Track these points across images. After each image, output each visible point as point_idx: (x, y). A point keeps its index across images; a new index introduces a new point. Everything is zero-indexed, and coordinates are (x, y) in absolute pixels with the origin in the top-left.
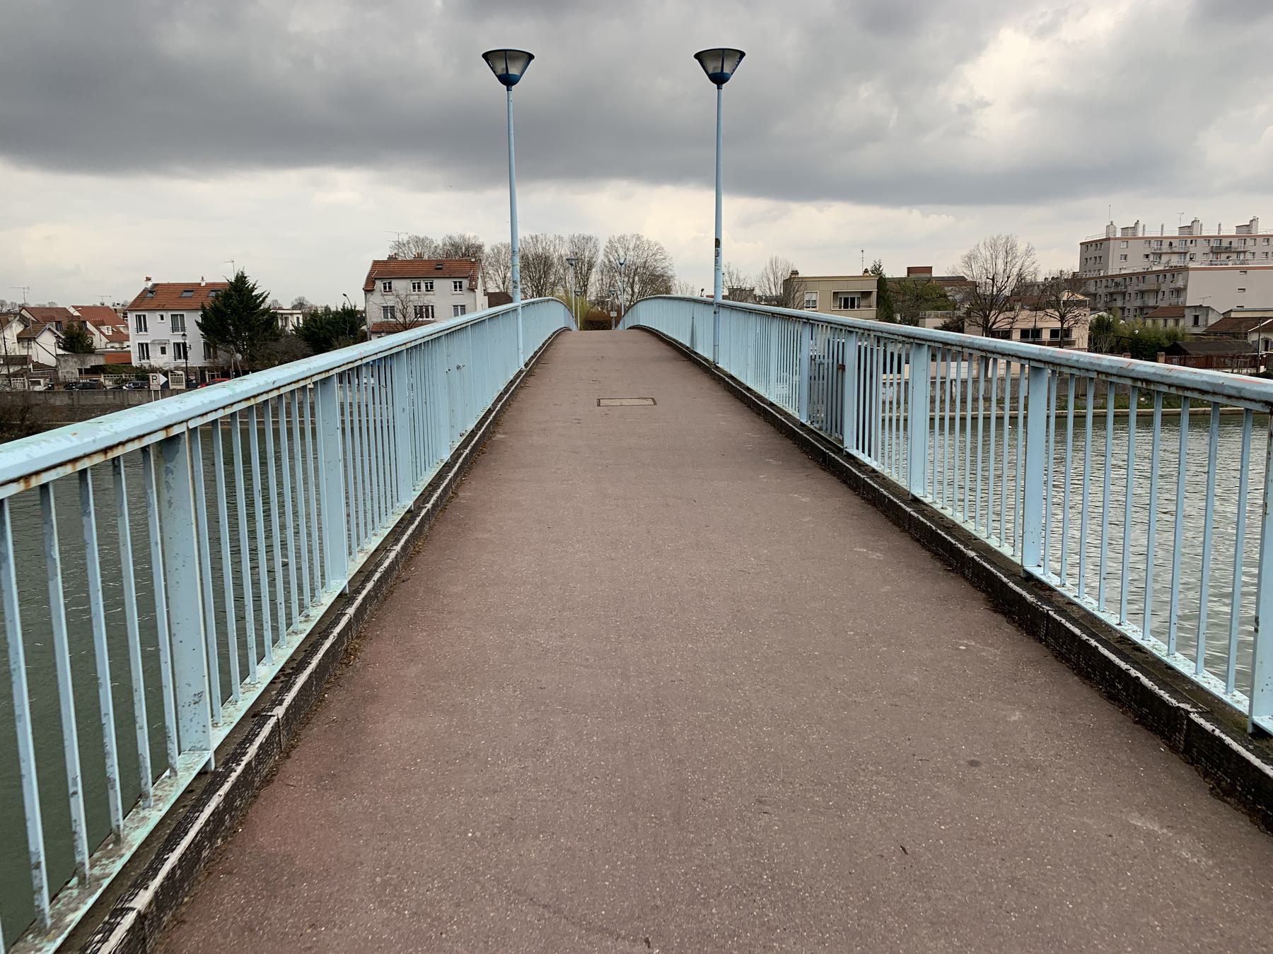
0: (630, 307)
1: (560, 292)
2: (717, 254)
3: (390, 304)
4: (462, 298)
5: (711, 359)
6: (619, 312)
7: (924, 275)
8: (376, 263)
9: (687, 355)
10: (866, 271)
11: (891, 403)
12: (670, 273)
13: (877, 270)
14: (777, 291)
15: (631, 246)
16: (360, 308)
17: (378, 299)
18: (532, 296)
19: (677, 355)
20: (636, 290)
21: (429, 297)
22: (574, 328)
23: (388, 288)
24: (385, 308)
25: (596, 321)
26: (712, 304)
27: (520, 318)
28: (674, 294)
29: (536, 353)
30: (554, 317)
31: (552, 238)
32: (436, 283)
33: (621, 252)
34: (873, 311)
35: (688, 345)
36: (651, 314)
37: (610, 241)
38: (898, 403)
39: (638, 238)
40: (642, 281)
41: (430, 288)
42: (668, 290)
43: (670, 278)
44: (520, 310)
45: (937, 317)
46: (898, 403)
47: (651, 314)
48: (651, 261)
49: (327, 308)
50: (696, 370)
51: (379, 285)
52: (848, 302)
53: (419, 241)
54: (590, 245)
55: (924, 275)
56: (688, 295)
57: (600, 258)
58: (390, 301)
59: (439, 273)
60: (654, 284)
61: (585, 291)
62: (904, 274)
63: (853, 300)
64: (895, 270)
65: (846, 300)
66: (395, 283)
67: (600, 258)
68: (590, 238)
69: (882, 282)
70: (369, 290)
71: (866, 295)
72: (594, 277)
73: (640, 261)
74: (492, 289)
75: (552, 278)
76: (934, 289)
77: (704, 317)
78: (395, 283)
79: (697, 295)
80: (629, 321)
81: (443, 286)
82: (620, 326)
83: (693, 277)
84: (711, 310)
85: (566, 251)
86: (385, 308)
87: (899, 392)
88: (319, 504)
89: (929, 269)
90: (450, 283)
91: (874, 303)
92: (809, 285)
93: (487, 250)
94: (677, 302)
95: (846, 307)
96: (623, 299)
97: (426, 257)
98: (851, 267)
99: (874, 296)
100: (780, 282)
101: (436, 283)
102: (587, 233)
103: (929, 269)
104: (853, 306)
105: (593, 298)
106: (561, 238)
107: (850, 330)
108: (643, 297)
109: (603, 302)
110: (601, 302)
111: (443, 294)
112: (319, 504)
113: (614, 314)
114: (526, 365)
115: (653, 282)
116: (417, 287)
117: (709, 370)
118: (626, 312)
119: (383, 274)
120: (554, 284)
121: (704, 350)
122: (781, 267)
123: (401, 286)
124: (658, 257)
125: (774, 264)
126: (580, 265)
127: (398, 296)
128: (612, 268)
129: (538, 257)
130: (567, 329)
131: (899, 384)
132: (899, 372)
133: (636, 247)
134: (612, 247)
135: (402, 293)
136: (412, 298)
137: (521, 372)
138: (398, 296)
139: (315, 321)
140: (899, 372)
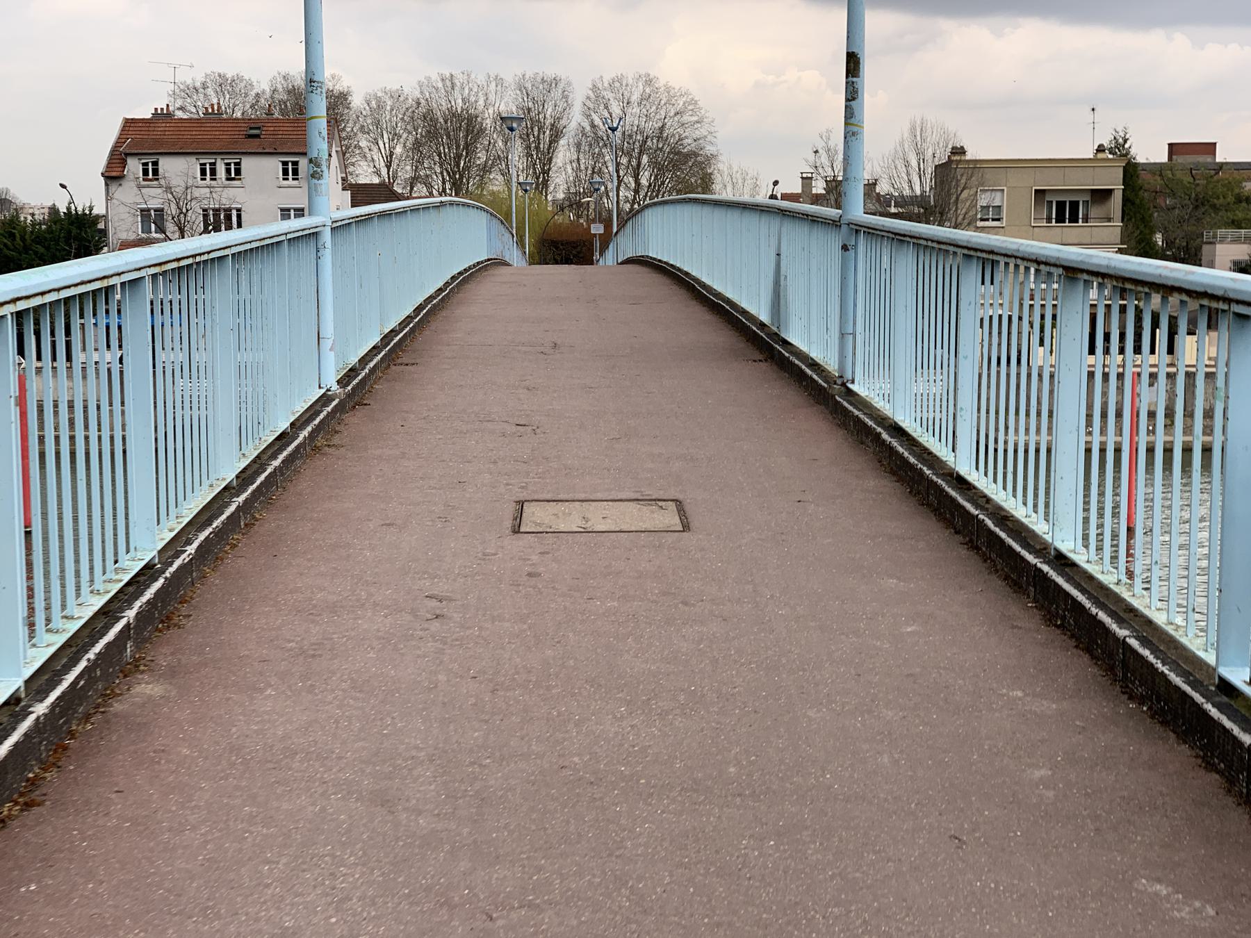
0: (633, 214)
1: (496, 183)
2: (852, 95)
3: (154, 204)
4: (295, 195)
5: (832, 365)
6: (608, 224)
7: (1202, 159)
8: (129, 124)
9: (763, 345)
10: (1101, 149)
11: (1152, 415)
12: (710, 150)
13: (1119, 149)
14: (920, 186)
15: (635, 98)
16: (99, 210)
17: (131, 195)
18: (443, 192)
19: (741, 344)
20: (644, 182)
21: (231, 192)
22: (515, 257)
23: (152, 173)
24: (145, 213)
25: (565, 246)
26: (835, 224)
27: (327, 255)
28: (722, 191)
29: (387, 338)
30: (465, 237)
31: (481, 79)
32: (248, 164)
33: (616, 110)
34: (1115, 228)
35: (764, 317)
36: (668, 235)
37: (594, 88)
38: (1170, 414)
39: (649, 82)
40: (654, 163)
41: (235, 173)
42: (706, 183)
43: (710, 159)
44: (327, 236)
45: (1237, 240)
46: (1170, 414)
47: (668, 235)
48: (672, 128)
49: (54, 210)
50: (790, 395)
51: (134, 167)
52: (1066, 210)
53: (224, 84)
54: (556, 94)
55: (1202, 159)
56: (746, 198)
57: (575, 120)
58: (155, 198)
59: (253, 145)
60: (679, 171)
61: (545, 184)
62: (1164, 158)
63: (1074, 205)
64: (1150, 150)
65: (1061, 205)
66: (165, 164)
67: (575, 120)
68: (556, 81)
69: (1131, 171)
70: (113, 175)
71: (1102, 196)
72: (563, 155)
73: (651, 126)
74: (365, 175)
75: (481, 157)
76: (1229, 186)
77: (811, 261)
78: (165, 164)
79: (762, 198)
80: (626, 246)
81: (261, 170)
82: (610, 258)
83: (762, 153)
84: (833, 241)
85: (508, 105)
86: (145, 213)
87: (1171, 396)
88: (30, 589)
89: (1210, 148)
90: (273, 165)
91: (1117, 212)
92: (989, 175)
93: (357, 101)
94: (733, 215)
95: (1060, 219)
96: (619, 196)
97: (238, 114)
98: (1073, 141)
99: (1117, 198)
100: (930, 170)
101: (248, 164)
102: (550, 73)
103: (1210, 148)
104: (1074, 219)
105: (561, 196)
106: (499, 81)
107: (1072, 273)
108: (655, 197)
109: (579, 204)
110: (573, 203)
111: (260, 188)
112: (30, 589)
113: (597, 229)
114: (342, 382)
115: (676, 166)
116: (208, 172)
117: (826, 396)
118: (622, 225)
119: (142, 144)
120: (486, 169)
121: (809, 336)
122: (932, 138)
123: (177, 170)
124: (686, 118)
125: (918, 133)
126: (534, 130)
127: (169, 189)
128: (597, 138)
129: (453, 115)
130: (498, 263)
131: (1171, 377)
132: (1171, 350)
133: (645, 99)
134: (597, 98)
135: (178, 183)
136: (197, 192)
137: (325, 399)
138: (169, 189)
139: (12, 236)
140: (1171, 350)
